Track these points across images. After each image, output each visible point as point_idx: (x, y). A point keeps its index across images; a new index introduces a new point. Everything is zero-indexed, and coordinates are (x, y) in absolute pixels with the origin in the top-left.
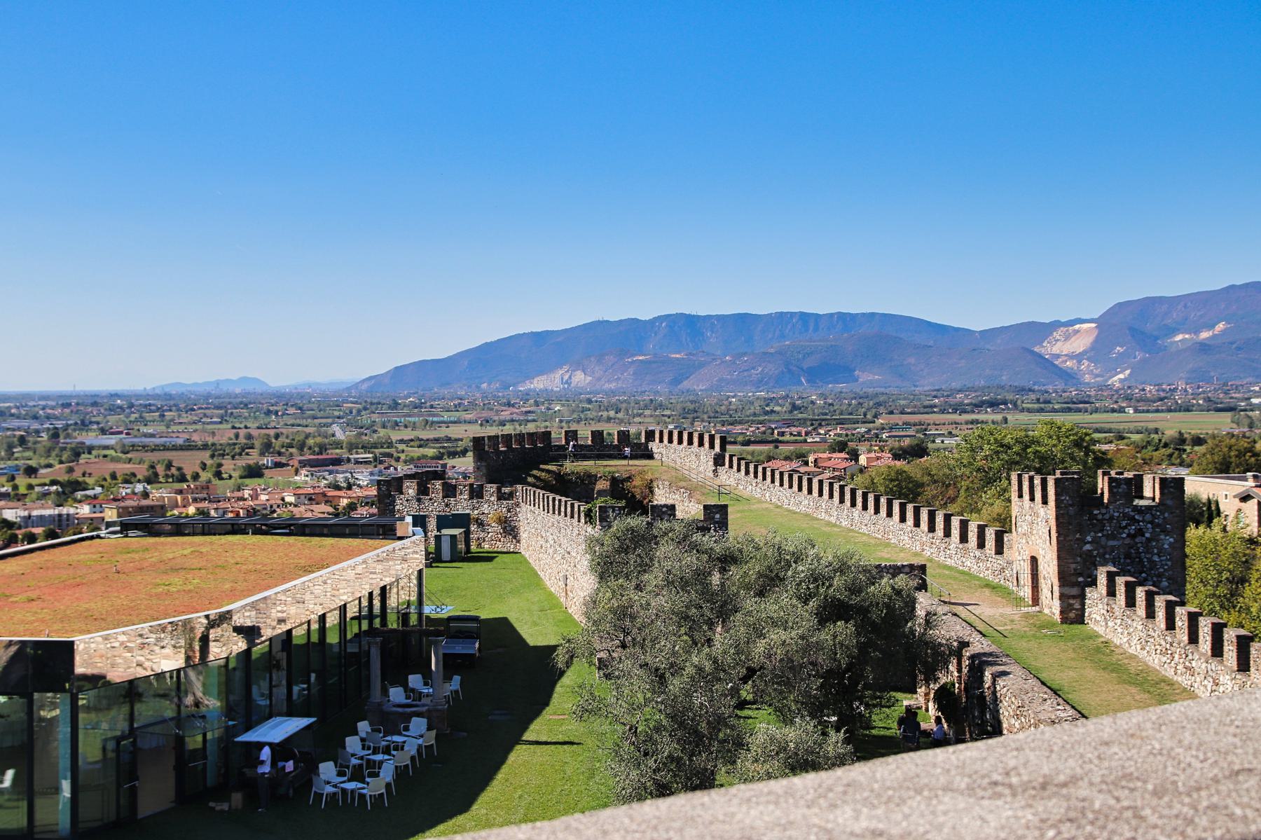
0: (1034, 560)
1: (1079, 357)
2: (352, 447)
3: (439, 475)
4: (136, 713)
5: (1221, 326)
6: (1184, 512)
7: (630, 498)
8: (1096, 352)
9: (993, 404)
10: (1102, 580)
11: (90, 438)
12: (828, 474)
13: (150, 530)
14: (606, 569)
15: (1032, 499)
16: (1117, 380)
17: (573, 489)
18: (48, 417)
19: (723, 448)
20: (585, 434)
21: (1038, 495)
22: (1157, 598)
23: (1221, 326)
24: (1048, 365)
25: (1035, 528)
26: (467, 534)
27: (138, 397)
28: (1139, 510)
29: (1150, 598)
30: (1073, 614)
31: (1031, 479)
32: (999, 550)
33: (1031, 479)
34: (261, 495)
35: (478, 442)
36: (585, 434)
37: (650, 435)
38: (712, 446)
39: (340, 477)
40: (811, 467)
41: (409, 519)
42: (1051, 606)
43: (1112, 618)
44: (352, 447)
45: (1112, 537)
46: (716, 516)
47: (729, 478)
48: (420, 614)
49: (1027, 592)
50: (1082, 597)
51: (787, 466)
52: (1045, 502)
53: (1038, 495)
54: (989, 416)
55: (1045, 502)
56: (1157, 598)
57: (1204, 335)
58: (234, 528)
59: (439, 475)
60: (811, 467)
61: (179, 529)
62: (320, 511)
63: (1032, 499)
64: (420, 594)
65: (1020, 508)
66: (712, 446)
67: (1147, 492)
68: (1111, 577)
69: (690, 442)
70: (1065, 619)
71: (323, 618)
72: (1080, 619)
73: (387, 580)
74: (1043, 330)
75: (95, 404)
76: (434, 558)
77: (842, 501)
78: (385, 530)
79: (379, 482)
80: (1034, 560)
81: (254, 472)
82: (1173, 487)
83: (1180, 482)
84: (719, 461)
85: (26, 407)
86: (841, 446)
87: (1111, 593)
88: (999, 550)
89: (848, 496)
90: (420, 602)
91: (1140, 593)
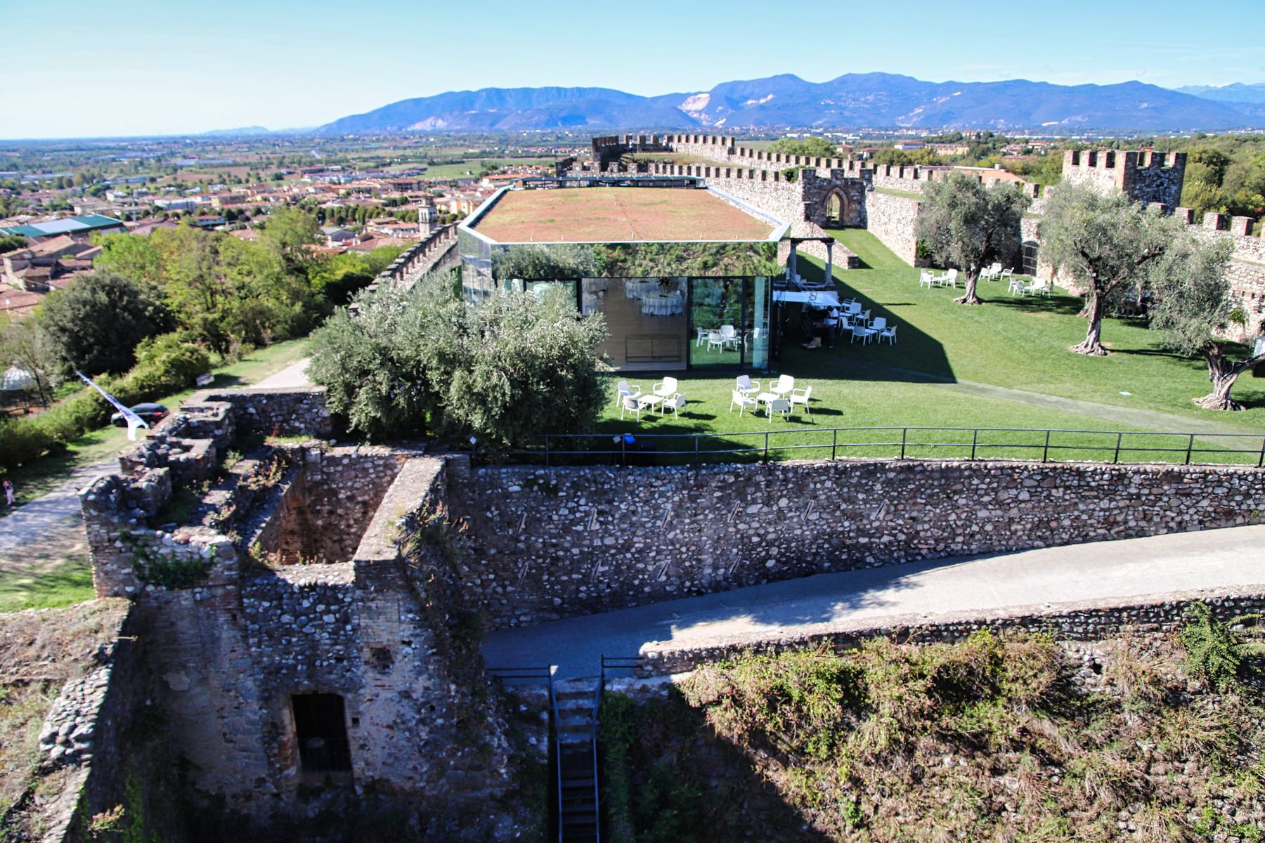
1: (700, 112)
2: (327, 163)
5: (770, 97)
8: (709, 109)
23: (770, 97)
28: (1163, 172)
74: (683, 97)
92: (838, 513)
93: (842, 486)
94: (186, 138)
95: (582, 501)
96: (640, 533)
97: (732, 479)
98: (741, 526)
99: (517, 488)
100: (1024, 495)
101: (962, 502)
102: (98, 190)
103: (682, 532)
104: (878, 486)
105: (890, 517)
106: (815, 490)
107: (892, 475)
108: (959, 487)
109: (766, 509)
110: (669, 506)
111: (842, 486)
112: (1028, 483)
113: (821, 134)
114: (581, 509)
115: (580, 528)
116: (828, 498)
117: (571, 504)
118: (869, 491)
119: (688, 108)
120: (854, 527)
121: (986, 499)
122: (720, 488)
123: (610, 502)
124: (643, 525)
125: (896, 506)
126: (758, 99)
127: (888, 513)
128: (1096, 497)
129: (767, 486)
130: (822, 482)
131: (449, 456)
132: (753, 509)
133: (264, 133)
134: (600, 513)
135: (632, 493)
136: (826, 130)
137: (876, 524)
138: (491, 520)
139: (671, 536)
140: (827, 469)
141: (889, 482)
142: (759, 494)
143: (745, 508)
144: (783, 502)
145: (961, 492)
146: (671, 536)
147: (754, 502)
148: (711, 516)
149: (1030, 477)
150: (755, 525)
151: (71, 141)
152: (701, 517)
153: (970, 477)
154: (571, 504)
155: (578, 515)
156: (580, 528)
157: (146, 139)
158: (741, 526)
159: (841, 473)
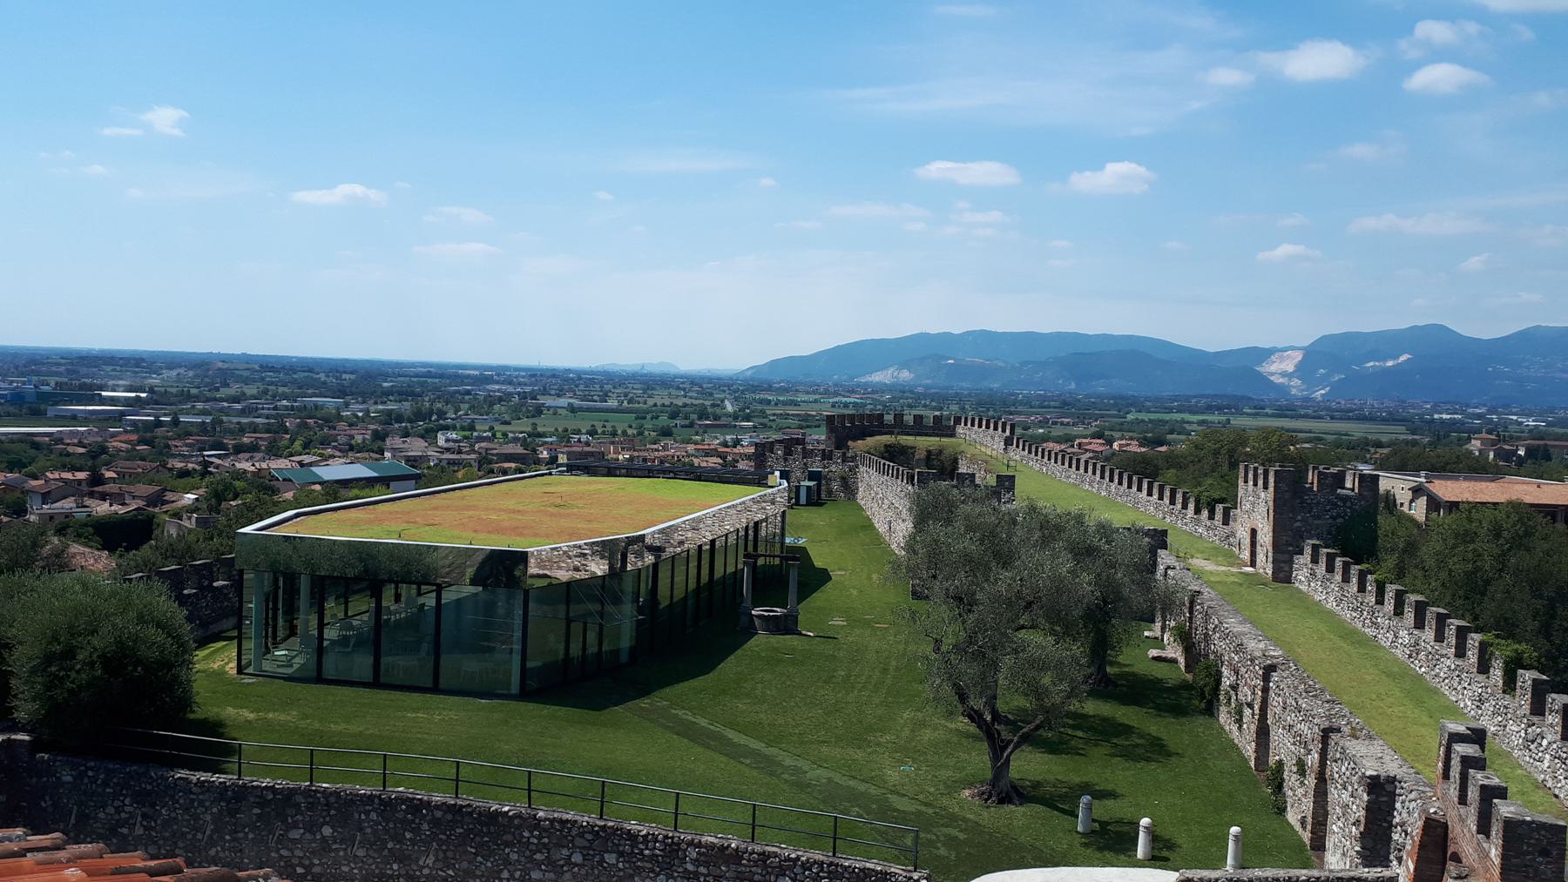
0: (1254, 532)
1: (1289, 375)
2: (736, 417)
3: (801, 442)
4: (382, 667)
5: (1403, 358)
6: (1373, 501)
7: (944, 467)
8: (1302, 370)
9: (1220, 409)
10: (1308, 550)
11: (549, 401)
12: (1088, 455)
13: (589, 471)
14: (921, 520)
15: (1255, 484)
16: (1319, 394)
17: (896, 456)
18: (520, 384)
19: (1012, 432)
20: (909, 419)
21: (1260, 482)
22: (1551, 697)
23: (1403, 358)
24: (1263, 380)
25: (1256, 510)
26: (819, 486)
27: (585, 373)
28: (1340, 497)
29: (1462, 633)
30: (1283, 574)
31: (1256, 469)
32: (1226, 522)
33: (1256, 469)
34: (673, 449)
35: (830, 419)
36: (909, 419)
37: (958, 421)
38: (1004, 431)
39: (728, 438)
40: (1076, 450)
41: (777, 473)
42: (1265, 566)
43: (1311, 578)
44: (736, 417)
45: (1318, 517)
46: (1006, 483)
47: (1016, 454)
48: (783, 543)
49: (1246, 555)
50: (1291, 562)
51: (1057, 448)
52: (1266, 487)
53: (1260, 482)
54: (1214, 418)
55: (1266, 487)
56: (1551, 697)
57: (1390, 363)
58: (649, 473)
59: (801, 442)
60: (1076, 450)
61: (612, 471)
62: (714, 461)
63: (1255, 484)
64: (783, 529)
65: (1245, 490)
66: (1004, 431)
67: (1348, 485)
68: (1315, 548)
69: (988, 427)
70: (1276, 578)
71: (713, 542)
72: (1288, 580)
73: (760, 516)
74: (1264, 354)
75: (554, 376)
76: (795, 500)
77: (1102, 477)
78: (760, 481)
79: (756, 445)
80: (1254, 532)
81: (666, 433)
82: (1370, 482)
83: (1375, 479)
84: (1008, 442)
85: (31, 363)
86: (1098, 435)
87: (1315, 560)
88: (1226, 522)
89: (1107, 474)
90: (783, 535)
91: (1339, 562)
92: (386, 852)
93: (388, 821)
94: (569, 371)
95: (127, 801)
96: (181, 844)
97: (271, 797)
98: (284, 852)
99: (69, 778)
100: (577, 858)
101: (514, 857)
102: (427, 431)
103: (223, 850)
104: (425, 826)
105: (440, 865)
106: (360, 821)
107: (439, 814)
108: (508, 837)
109: (308, 836)
110: (208, 818)
111: (388, 821)
112: (579, 842)
113: (1479, 416)
114: (127, 809)
115: (125, 831)
116: (375, 832)
117: (117, 803)
118: (416, 831)
119: (1273, 368)
120: (403, 872)
121: (538, 856)
122: (259, 805)
123: (153, 805)
124: (184, 834)
125: (445, 852)
126: (1385, 360)
127: (437, 860)
128: (653, 871)
129: (308, 809)
130: (367, 813)
131: (1315, 873)
132: (295, 834)
133: (673, 371)
134: (144, 816)
135: (172, 797)
136: (1490, 412)
137: (426, 871)
138: (45, 810)
139: (212, 852)
140: (371, 798)
141: (435, 823)
142: (299, 817)
143: (287, 831)
144: (327, 831)
145: (514, 845)
146: (212, 852)
147: (295, 826)
148: (251, 836)
149: (581, 835)
150: (298, 853)
151: (424, 365)
152: (241, 835)
153: (519, 827)
154: (117, 803)
155: (123, 815)
156: (125, 831)
157: (516, 369)
158: (284, 852)
159: (387, 806)
